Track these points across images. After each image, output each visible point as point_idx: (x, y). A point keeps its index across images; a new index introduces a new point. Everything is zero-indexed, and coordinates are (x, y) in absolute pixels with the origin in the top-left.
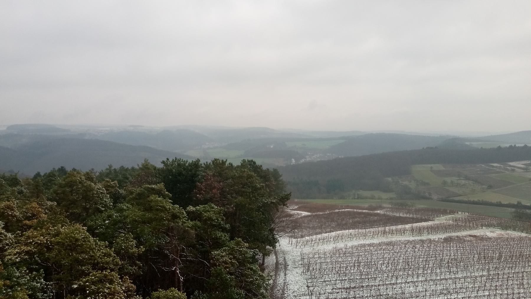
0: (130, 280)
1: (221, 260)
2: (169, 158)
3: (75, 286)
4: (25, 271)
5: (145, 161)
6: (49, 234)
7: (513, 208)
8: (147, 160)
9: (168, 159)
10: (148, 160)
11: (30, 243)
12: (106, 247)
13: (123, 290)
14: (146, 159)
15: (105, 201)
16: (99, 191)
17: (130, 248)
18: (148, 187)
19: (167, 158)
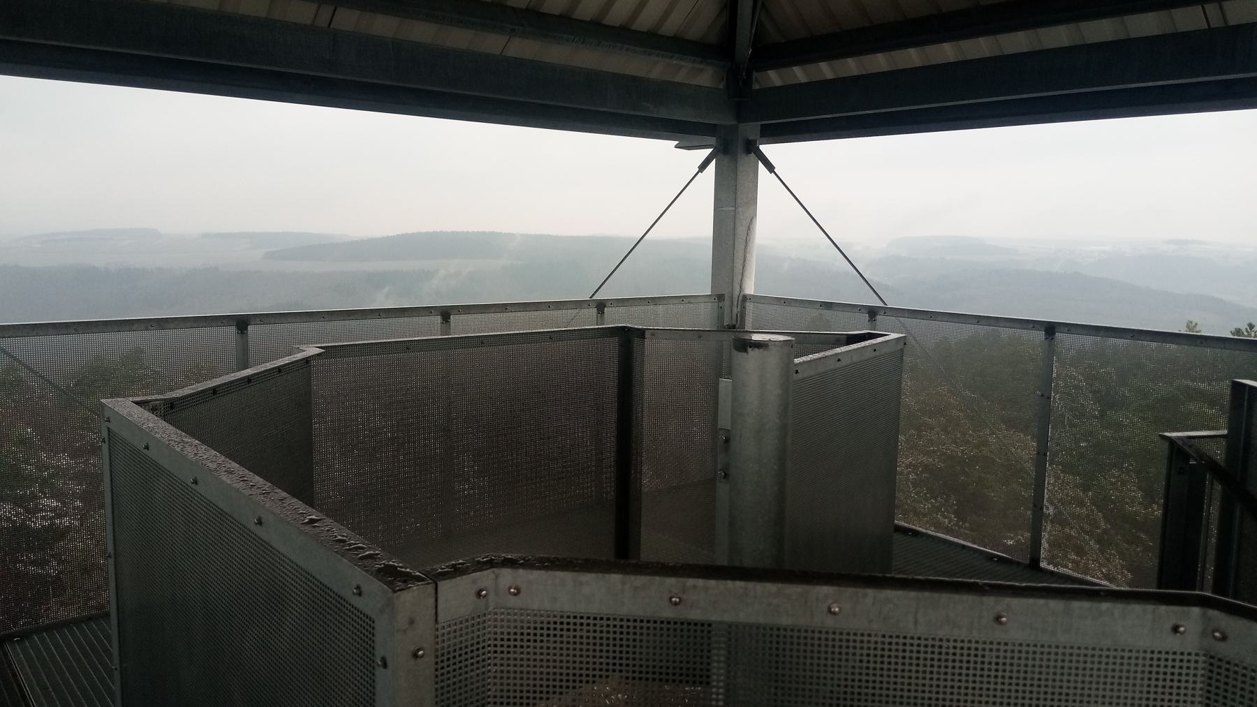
0: (1120, 559)
1: (489, 513)
2: (1253, 323)
3: (1010, 542)
4: (925, 494)
5: (1188, 326)
6: (968, 442)
7: (893, 579)
8: (1194, 324)
9: (1251, 326)
10: (1196, 324)
11: (934, 451)
12: (1076, 486)
13: (1102, 573)
14: (1191, 322)
15: (1083, 405)
16: (1071, 382)
17: (1127, 503)
18: (1187, 386)
19: (1248, 322)
